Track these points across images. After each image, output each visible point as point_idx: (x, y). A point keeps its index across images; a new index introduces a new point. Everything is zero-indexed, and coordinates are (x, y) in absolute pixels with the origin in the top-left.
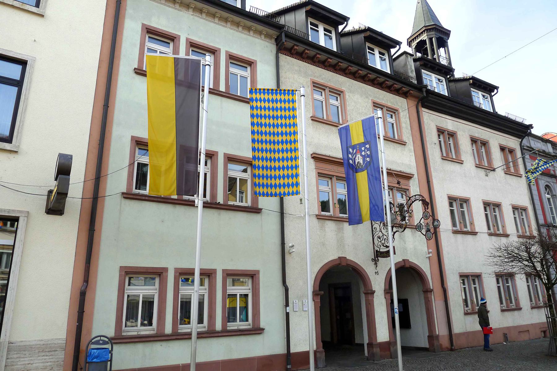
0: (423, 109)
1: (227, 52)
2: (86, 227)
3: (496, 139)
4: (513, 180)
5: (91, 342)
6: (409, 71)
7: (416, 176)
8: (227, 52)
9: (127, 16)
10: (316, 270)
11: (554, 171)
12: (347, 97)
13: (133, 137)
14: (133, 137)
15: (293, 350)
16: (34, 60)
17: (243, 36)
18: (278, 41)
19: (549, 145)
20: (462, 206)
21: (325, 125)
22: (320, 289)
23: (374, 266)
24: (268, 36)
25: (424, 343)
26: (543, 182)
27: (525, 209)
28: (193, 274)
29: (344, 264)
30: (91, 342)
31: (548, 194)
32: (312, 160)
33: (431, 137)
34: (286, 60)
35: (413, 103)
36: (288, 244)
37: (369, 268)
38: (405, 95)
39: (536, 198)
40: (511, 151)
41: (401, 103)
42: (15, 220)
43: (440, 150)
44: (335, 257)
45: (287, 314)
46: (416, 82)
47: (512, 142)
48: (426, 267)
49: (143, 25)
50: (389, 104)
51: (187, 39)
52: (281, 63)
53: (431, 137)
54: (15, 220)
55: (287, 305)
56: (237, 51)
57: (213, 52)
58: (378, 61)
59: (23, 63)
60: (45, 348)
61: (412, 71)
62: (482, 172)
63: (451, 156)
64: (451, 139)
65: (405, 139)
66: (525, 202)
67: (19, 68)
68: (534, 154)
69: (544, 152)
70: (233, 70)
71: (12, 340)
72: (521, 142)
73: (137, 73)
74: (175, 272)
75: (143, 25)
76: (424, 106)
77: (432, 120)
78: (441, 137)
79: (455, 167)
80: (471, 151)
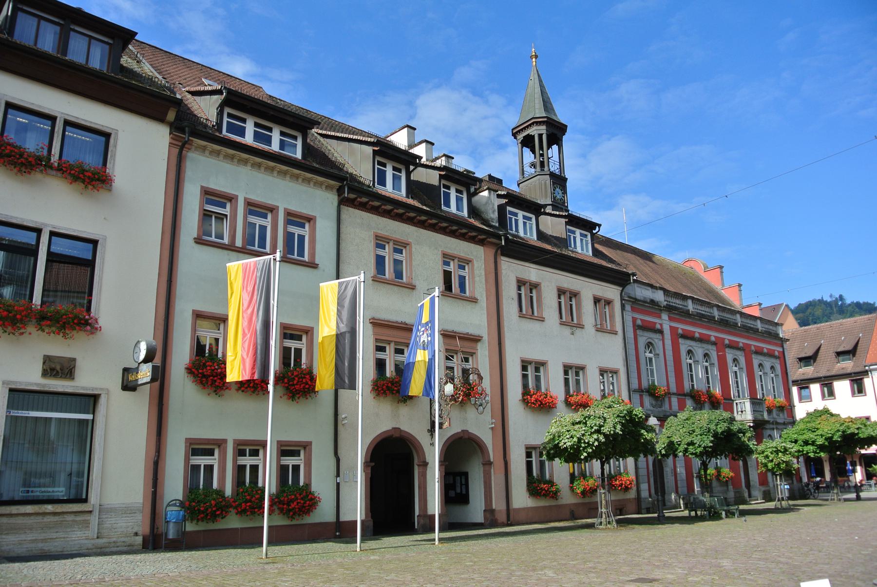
0: (503, 258)
1: (285, 209)
2: (156, 401)
3: (589, 289)
4: (606, 338)
5: (168, 505)
6: (491, 211)
7: (485, 337)
8: (285, 209)
9: (186, 179)
10: (369, 441)
11: (661, 325)
12: (413, 250)
13: (193, 311)
14: (193, 311)
15: (343, 518)
16: (105, 239)
17: (291, 184)
18: (340, 191)
19: (661, 293)
20: (577, 374)
21: (386, 285)
22: (371, 461)
23: (430, 437)
24: (329, 188)
25: (479, 518)
26: (645, 338)
27: (615, 372)
28: (264, 446)
29: (397, 435)
30: (168, 505)
31: (651, 352)
32: (370, 325)
33: (509, 290)
34: (352, 215)
35: (491, 252)
36: (342, 416)
37: (422, 438)
38: (481, 242)
39: (632, 358)
40: (608, 302)
41: (478, 254)
42: (95, 398)
43: (557, 313)
44: (389, 428)
45: (338, 485)
46: (497, 225)
47: (611, 292)
48: (487, 438)
49: (202, 187)
50: (462, 255)
51: (245, 199)
52: (344, 216)
53: (509, 290)
54: (95, 398)
55: (338, 475)
56: (258, 197)
57: (272, 209)
58: (455, 205)
59: (95, 243)
60: (128, 511)
61: (494, 212)
62: (567, 331)
63: (529, 310)
64: (607, 307)
65: (477, 296)
66: (617, 362)
67: (34, 235)
68: (637, 304)
69: (652, 302)
70: (252, 219)
71: (102, 503)
72: (622, 291)
73: (196, 242)
74: (234, 443)
75: (202, 187)
76: (503, 255)
77: (512, 270)
78: (562, 297)
79: (535, 326)
80: (557, 305)
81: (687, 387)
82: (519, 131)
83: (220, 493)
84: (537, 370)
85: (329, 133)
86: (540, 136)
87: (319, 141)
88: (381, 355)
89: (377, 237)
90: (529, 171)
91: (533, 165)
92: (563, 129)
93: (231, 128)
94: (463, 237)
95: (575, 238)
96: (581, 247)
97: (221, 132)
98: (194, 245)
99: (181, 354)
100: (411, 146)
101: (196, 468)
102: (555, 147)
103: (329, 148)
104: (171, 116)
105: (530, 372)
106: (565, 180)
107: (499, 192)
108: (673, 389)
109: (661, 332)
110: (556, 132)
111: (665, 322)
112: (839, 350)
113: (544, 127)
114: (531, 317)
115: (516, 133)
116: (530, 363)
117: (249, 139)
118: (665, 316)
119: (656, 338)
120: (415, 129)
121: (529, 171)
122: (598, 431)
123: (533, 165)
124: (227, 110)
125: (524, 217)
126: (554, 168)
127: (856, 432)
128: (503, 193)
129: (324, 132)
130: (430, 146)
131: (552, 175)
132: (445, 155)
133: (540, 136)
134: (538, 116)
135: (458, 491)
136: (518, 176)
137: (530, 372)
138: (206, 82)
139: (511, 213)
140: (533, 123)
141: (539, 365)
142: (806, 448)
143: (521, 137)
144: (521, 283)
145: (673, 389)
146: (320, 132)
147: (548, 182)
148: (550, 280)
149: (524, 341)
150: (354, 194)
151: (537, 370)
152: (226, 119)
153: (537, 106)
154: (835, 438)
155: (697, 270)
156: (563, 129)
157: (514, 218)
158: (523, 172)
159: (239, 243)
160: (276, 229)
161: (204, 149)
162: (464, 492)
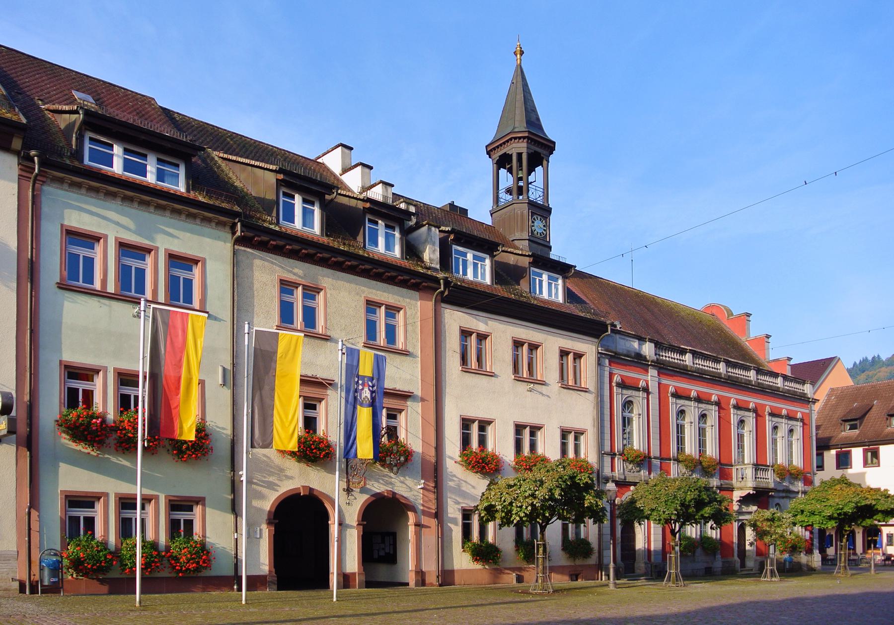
3: (552, 342)
22: (274, 518)
33: (452, 342)
46: (438, 267)
51: (116, 239)
53: (452, 342)
62: (523, 387)
77: (455, 319)
81: (618, 447)
82: (494, 149)
83: (104, 544)
84: (533, 434)
85: (230, 157)
86: (520, 155)
87: (219, 167)
88: (311, 413)
89: (283, 282)
90: (505, 197)
91: (509, 191)
92: (550, 147)
93: (94, 156)
94: (391, 281)
95: (541, 282)
96: (550, 290)
97: (81, 160)
98: (58, 290)
99: (51, 407)
100: (345, 171)
101: (75, 520)
102: (539, 169)
103: (231, 175)
104: (17, 144)
105: (571, 437)
106: (548, 211)
107: (443, 228)
108: (655, 451)
109: (646, 390)
110: (540, 150)
111: (651, 377)
112: (220, 381)
113: (525, 145)
114: (481, 371)
115: (491, 150)
116: (525, 427)
117: (117, 168)
118: (653, 372)
119: (639, 398)
120: (351, 149)
121: (505, 197)
122: (533, 496)
123: (509, 191)
124: (89, 135)
125: (475, 257)
126: (535, 194)
127: (874, 503)
128: (447, 229)
129: (225, 156)
130: (367, 170)
131: (532, 204)
132: (381, 182)
133: (520, 155)
134: (516, 130)
135: (387, 551)
136: (489, 204)
137: (571, 437)
138: (77, 95)
139: (458, 252)
140: (511, 139)
141: (535, 430)
142: (812, 519)
143: (497, 155)
144: (465, 334)
145: (655, 451)
146: (221, 155)
147: (526, 212)
148: (502, 332)
149: (464, 397)
150: (257, 233)
151: (533, 434)
152: (87, 145)
153: (518, 118)
154: (846, 509)
155: (719, 316)
156: (550, 147)
157: (461, 258)
158: (497, 199)
159: (111, 289)
160: (155, 272)
161: (61, 181)
162: (392, 552)
